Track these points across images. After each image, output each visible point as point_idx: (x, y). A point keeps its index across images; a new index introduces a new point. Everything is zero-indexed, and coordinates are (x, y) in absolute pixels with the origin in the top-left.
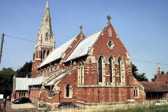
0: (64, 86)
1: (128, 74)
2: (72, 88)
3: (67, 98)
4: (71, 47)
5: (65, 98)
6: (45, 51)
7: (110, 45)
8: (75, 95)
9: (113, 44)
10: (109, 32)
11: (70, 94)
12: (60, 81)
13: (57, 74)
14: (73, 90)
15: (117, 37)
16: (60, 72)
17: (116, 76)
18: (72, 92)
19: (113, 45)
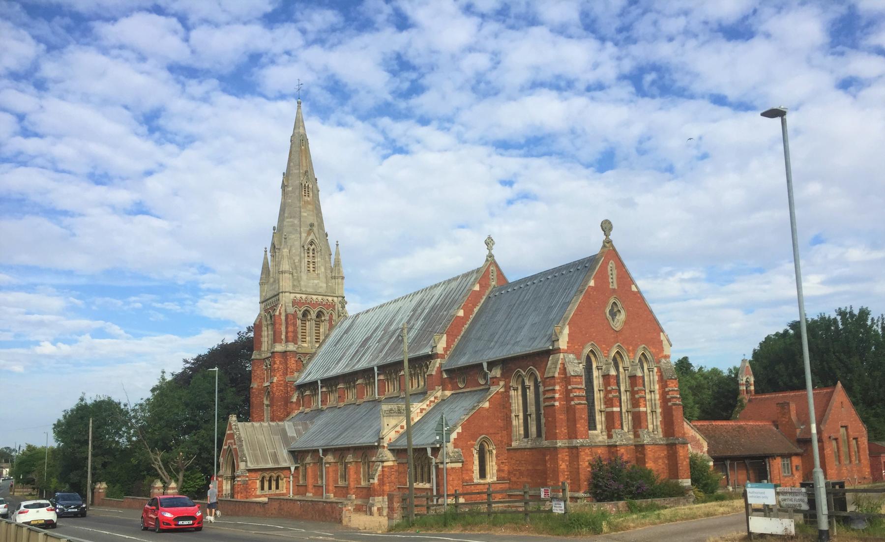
0: (473, 446)
1: (670, 404)
2: (494, 452)
3: (482, 481)
5: (476, 481)
6: (305, 314)
7: (613, 314)
9: (623, 312)
10: (610, 272)
11: (488, 468)
12: (459, 430)
14: (497, 456)
15: (634, 288)
16: (432, 399)
17: (637, 410)
18: (494, 463)
19: (622, 317)
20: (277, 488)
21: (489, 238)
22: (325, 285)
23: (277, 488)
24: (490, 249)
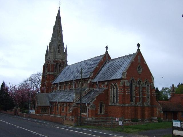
2: (104, 106)
4: (98, 67)
7: (139, 69)
8: (106, 111)
11: (102, 110)
12: (95, 99)
13: (86, 92)
18: (104, 109)
19: (141, 70)
20: (46, 111)
21: (107, 46)
22: (62, 57)
23: (46, 111)
24: (107, 49)
